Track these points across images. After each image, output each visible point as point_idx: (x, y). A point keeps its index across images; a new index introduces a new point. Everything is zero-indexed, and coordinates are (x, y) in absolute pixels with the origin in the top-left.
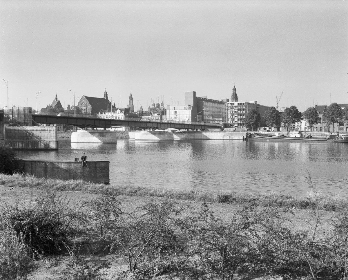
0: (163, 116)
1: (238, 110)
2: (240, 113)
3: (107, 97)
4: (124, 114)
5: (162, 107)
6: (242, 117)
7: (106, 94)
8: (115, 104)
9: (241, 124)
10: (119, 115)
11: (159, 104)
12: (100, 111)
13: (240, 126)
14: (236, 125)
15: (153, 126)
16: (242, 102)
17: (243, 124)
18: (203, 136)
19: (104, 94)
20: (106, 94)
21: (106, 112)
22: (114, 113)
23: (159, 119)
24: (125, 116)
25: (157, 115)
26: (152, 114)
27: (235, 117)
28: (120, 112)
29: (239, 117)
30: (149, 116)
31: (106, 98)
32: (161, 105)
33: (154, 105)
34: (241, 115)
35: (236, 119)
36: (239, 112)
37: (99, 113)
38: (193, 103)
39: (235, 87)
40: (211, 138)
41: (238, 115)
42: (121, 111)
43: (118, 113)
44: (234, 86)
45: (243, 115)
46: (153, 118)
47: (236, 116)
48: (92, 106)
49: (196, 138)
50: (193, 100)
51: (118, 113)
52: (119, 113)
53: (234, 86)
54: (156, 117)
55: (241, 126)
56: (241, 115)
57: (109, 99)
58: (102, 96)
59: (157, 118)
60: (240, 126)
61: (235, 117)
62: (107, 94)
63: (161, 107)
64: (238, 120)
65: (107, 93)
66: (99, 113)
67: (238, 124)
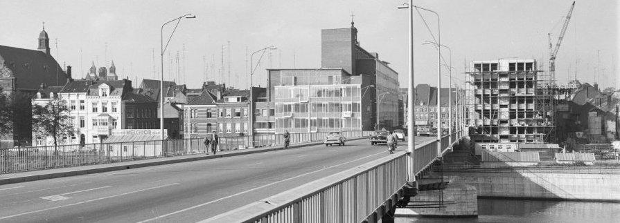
0: (258, 103)
1: (512, 85)
2: (517, 95)
3: (48, 49)
4: (123, 97)
5: (113, 75)
6: (523, 106)
7: (45, 40)
8: (69, 68)
9: (521, 130)
10: (104, 99)
11: (105, 68)
12: (40, 88)
13: (519, 136)
14: (506, 133)
15: (520, 147)
16: (525, 61)
17: (519, 128)
18: (527, 186)
19: (40, 40)
20: (45, 40)
21: (59, 90)
22: (89, 94)
23: (245, 113)
24: (126, 103)
25: (238, 99)
26: (219, 98)
27: (502, 106)
28: (108, 92)
29: (515, 107)
30: (210, 103)
31: (44, 50)
32: (111, 72)
33: (93, 70)
34: (521, 100)
35: (505, 114)
36: (515, 90)
37: (39, 94)
38: (350, 65)
39: (355, 26)
40: (564, 196)
41: (513, 100)
42: (112, 89)
43: (100, 94)
44: (353, 23)
45: (529, 100)
46: (225, 110)
47: (503, 103)
48: (14, 72)
49: (497, 192)
50: (350, 53)
51: (100, 94)
52: (104, 95)
53: (353, 23)
54: (233, 105)
55: (523, 136)
56: (521, 100)
57: (52, 53)
58: (34, 45)
59: (238, 110)
60: (519, 136)
61: (502, 106)
62: (47, 40)
63: (108, 74)
64: (512, 116)
65: (46, 35)
66: (39, 94)
67: (513, 130)
